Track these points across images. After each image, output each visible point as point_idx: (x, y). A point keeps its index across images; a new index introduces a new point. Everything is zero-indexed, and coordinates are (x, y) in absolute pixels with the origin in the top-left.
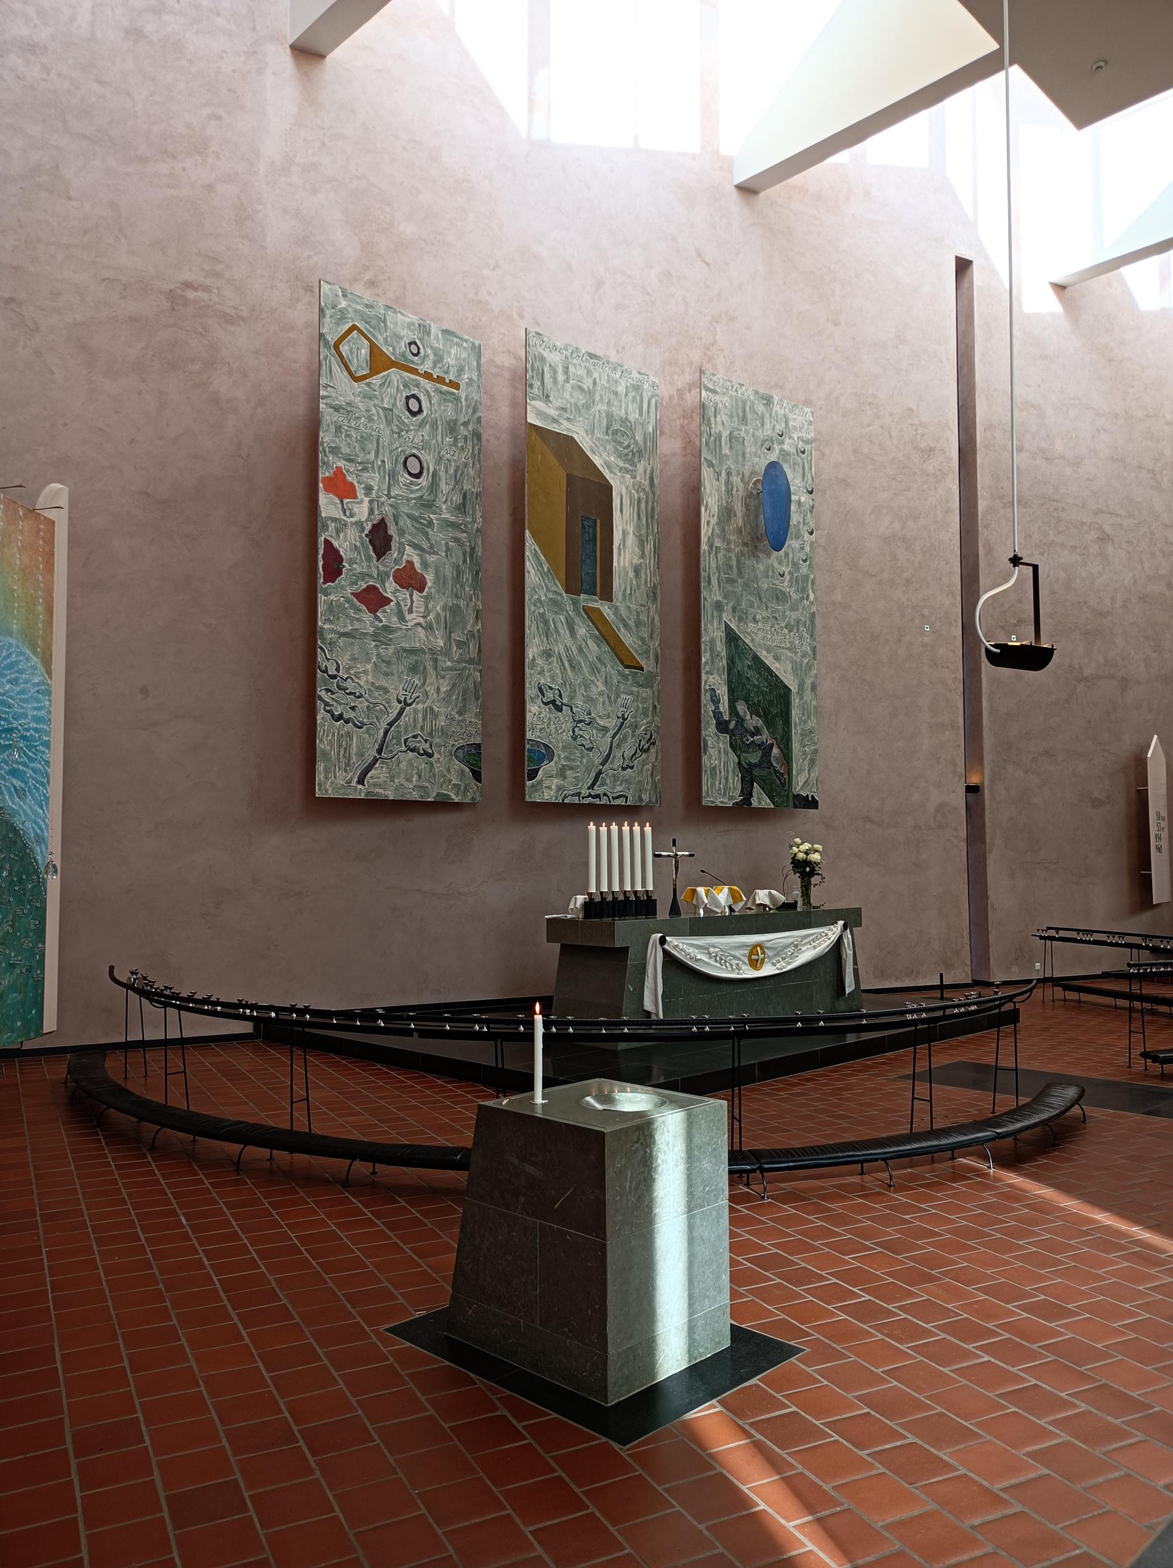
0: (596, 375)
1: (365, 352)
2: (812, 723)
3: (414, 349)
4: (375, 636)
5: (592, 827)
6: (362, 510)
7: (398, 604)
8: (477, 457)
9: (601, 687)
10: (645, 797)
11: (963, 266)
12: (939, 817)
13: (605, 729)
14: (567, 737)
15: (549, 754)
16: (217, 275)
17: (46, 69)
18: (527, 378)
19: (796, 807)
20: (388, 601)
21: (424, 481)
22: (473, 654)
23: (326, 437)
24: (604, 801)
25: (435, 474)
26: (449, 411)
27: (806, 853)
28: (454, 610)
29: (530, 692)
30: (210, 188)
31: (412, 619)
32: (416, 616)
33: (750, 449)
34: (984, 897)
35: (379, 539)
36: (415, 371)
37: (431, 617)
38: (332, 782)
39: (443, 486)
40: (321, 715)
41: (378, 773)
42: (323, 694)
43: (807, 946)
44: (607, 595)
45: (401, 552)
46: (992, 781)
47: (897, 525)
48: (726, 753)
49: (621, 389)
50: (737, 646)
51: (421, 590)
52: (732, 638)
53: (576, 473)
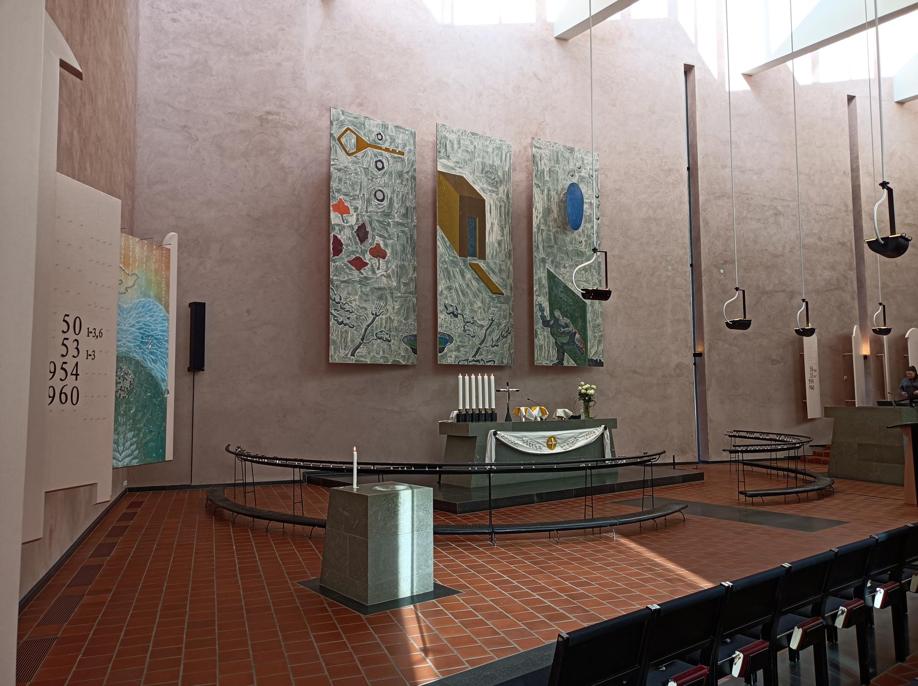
0: (475, 143)
1: (354, 141)
2: (599, 321)
3: (380, 137)
4: (360, 282)
5: (460, 377)
6: (352, 220)
7: (372, 266)
8: (414, 189)
9: (480, 304)
10: (505, 361)
11: (688, 69)
12: (677, 371)
13: (482, 326)
14: (460, 330)
15: (451, 340)
16: (282, 107)
17: (201, 15)
18: (440, 147)
19: (590, 365)
20: (367, 264)
21: (385, 203)
22: (412, 289)
23: (334, 185)
24: (482, 363)
25: (391, 199)
26: (399, 167)
27: (586, 390)
28: (402, 267)
29: (440, 308)
30: (279, 64)
31: (379, 273)
32: (381, 271)
33: (561, 176)
34: (705, 414)
35: (362, 233)
36: (380, 148)
37: (390, 271)
38: (338, 355)
39: (396, 205)
40: (332, 322)
41: (362, 351)
42: (333, 311)
43: (584, 437)
44: (483, 256)
45: (373, 239)
46: (709, 350)
47: (651, 212)
48: (548, 338)
49: (490, 150)
50: (554, 281)
51: (384, 258)
52: (551, 277)
53: (465, 194)
